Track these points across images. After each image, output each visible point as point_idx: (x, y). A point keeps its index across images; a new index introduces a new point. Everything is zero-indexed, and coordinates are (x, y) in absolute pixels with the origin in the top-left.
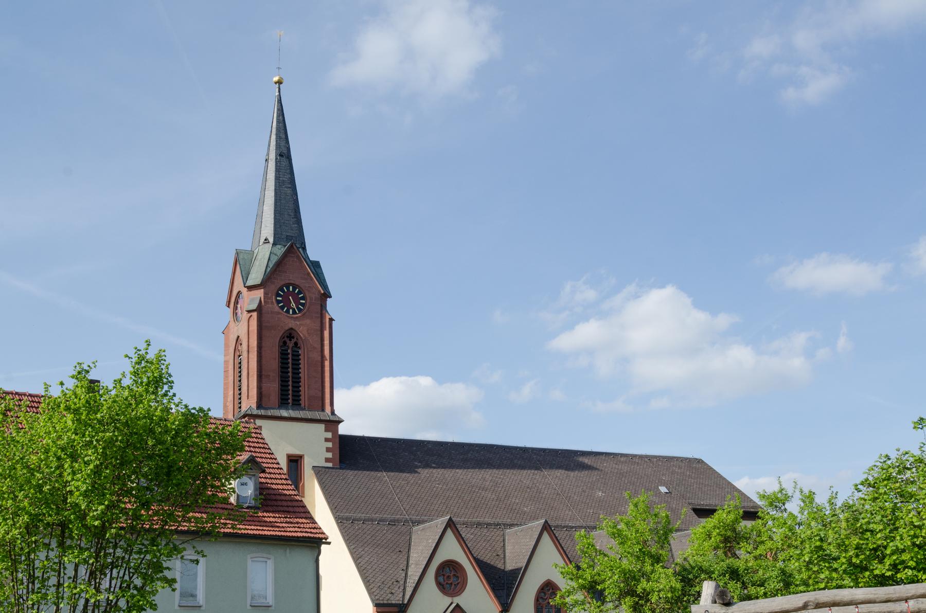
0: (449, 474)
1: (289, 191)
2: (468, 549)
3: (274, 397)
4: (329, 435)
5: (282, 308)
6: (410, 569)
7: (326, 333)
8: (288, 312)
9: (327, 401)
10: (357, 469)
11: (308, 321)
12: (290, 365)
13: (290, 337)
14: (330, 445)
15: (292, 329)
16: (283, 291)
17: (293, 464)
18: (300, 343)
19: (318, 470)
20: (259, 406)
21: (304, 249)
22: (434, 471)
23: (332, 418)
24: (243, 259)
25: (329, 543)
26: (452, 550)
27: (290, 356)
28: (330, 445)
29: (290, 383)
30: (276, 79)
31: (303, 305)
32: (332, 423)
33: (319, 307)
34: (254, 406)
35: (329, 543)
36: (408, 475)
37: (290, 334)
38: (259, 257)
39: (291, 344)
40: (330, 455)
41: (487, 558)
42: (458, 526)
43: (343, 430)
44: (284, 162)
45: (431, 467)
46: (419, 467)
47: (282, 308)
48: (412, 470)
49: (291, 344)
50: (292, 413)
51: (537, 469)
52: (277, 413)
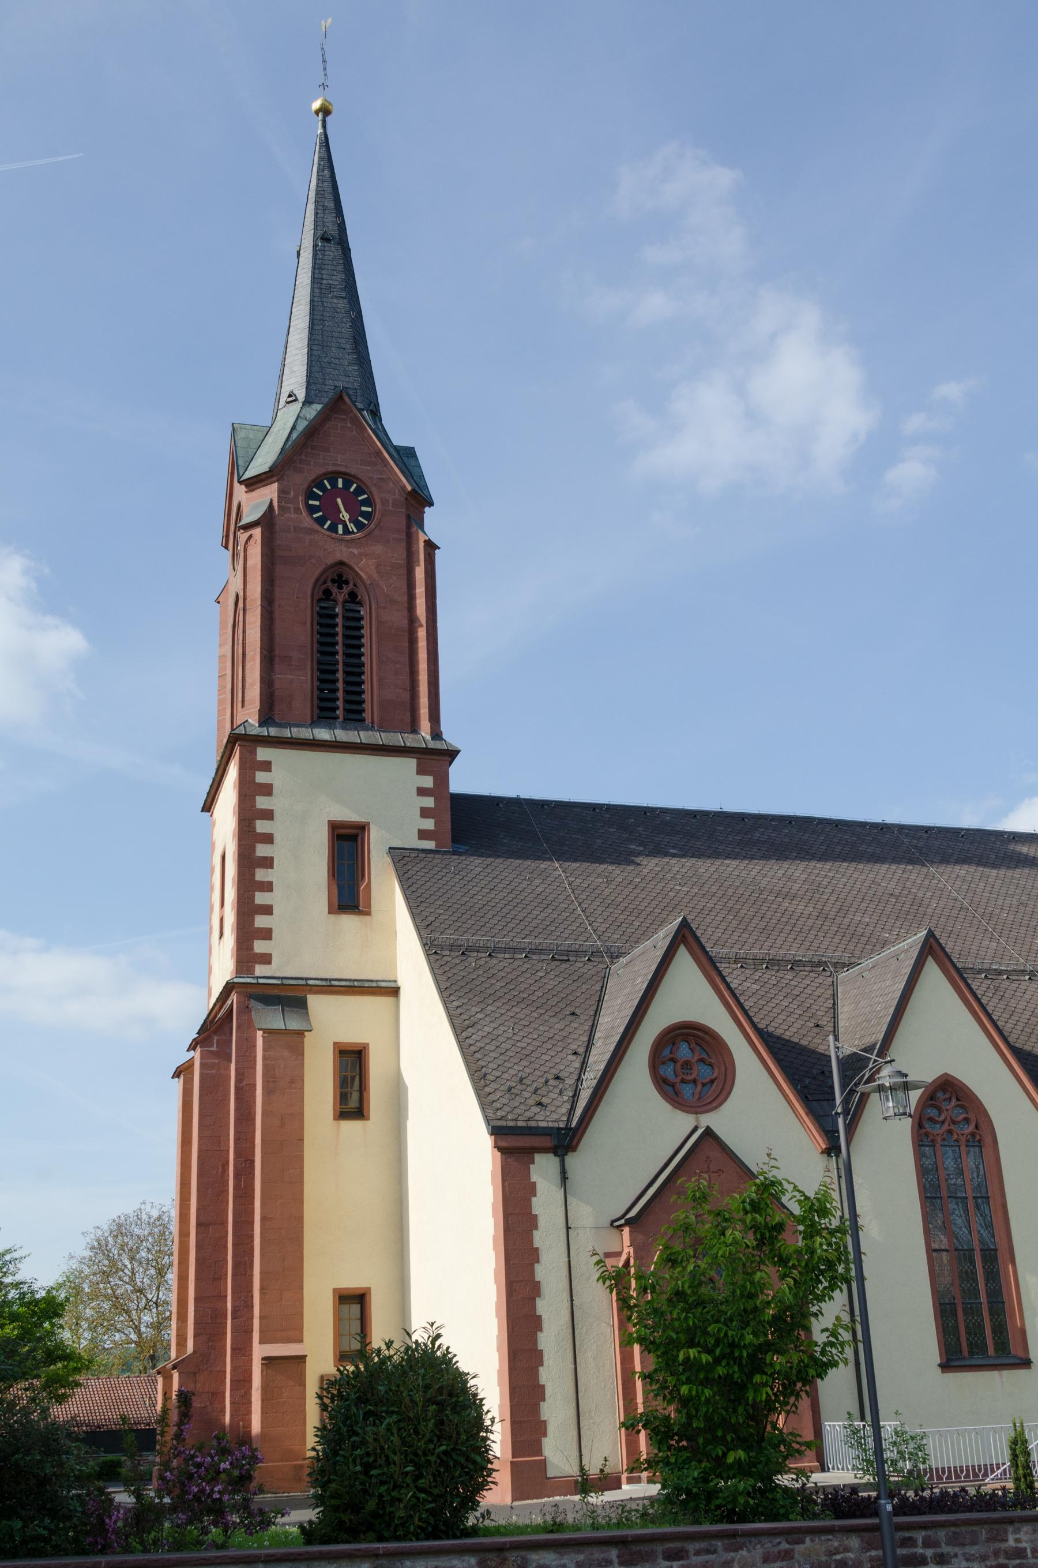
0: (706, 868)
1: (342, 305)
2: (745, 1012)
3: (302, 701)
4: (428, 782)
5: (321, 521)
6: (594, 1051)
7: (420, 573)
8: (333, 528)
9: (424, 711)
10: (496, 855)
11: (378, 549)
12: (339, 639)
13: (340, 581)
15: (341, 563)
16: (322, 488)
17: (346, 845)
18: (362, 593)
19: (400, 857)
20: (266, 719)
21: (375, 413)
22: (674, 861)
23: (433, 745)
24: (246, 438)
26: (690, 997)
27: (339, 620)
29: (340, 675)
30: (316, 105)
31: (368, 516)
32: (438, 758)
34: (254, 721)
36: (611, 868)
37: (340, 576)
40: (429, 824)
41: (792, 1029)
42: (721, 966)
43: (463, 779)
44: (333, 251)
45: (666, 854)
46: (640, 854)
47: (321, 521)
48: (624, 858)
50: (342, 735)
51: (911, 861)
52: (305, 733)
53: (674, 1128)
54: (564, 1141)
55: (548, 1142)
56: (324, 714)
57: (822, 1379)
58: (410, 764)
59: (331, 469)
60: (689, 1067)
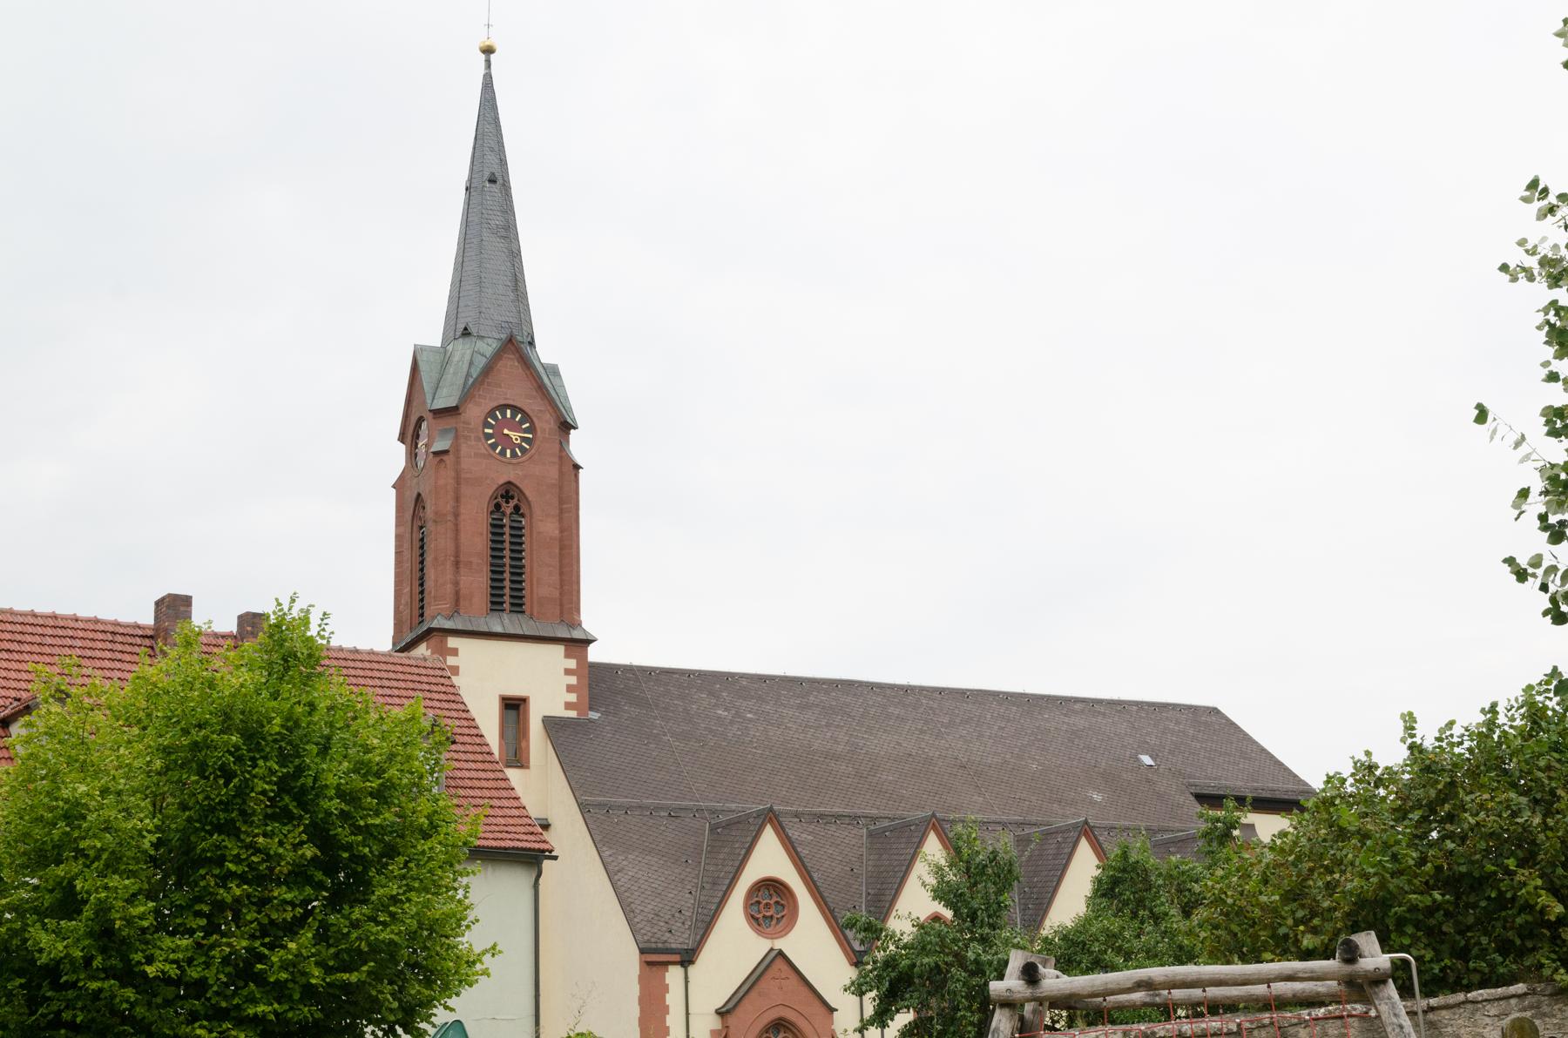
14: (573, 680)
15: (509, 483)
17: (512, 713)
25: (555, 858)
28: (573, 680)
32: (578, 645)
33: (557, 446)
35: (555, 858)
38: (456, 359)
39: (508, 508)
40: (573, 698)
43: (595, 654)
49: (508, 508)
53: (755, 948)
54: (687, 958)
55: (677, 958)
56: (496, 605)
57: (1366, 769)
58: (559, 650)
59: (503, 402)
60: (770, 904)
